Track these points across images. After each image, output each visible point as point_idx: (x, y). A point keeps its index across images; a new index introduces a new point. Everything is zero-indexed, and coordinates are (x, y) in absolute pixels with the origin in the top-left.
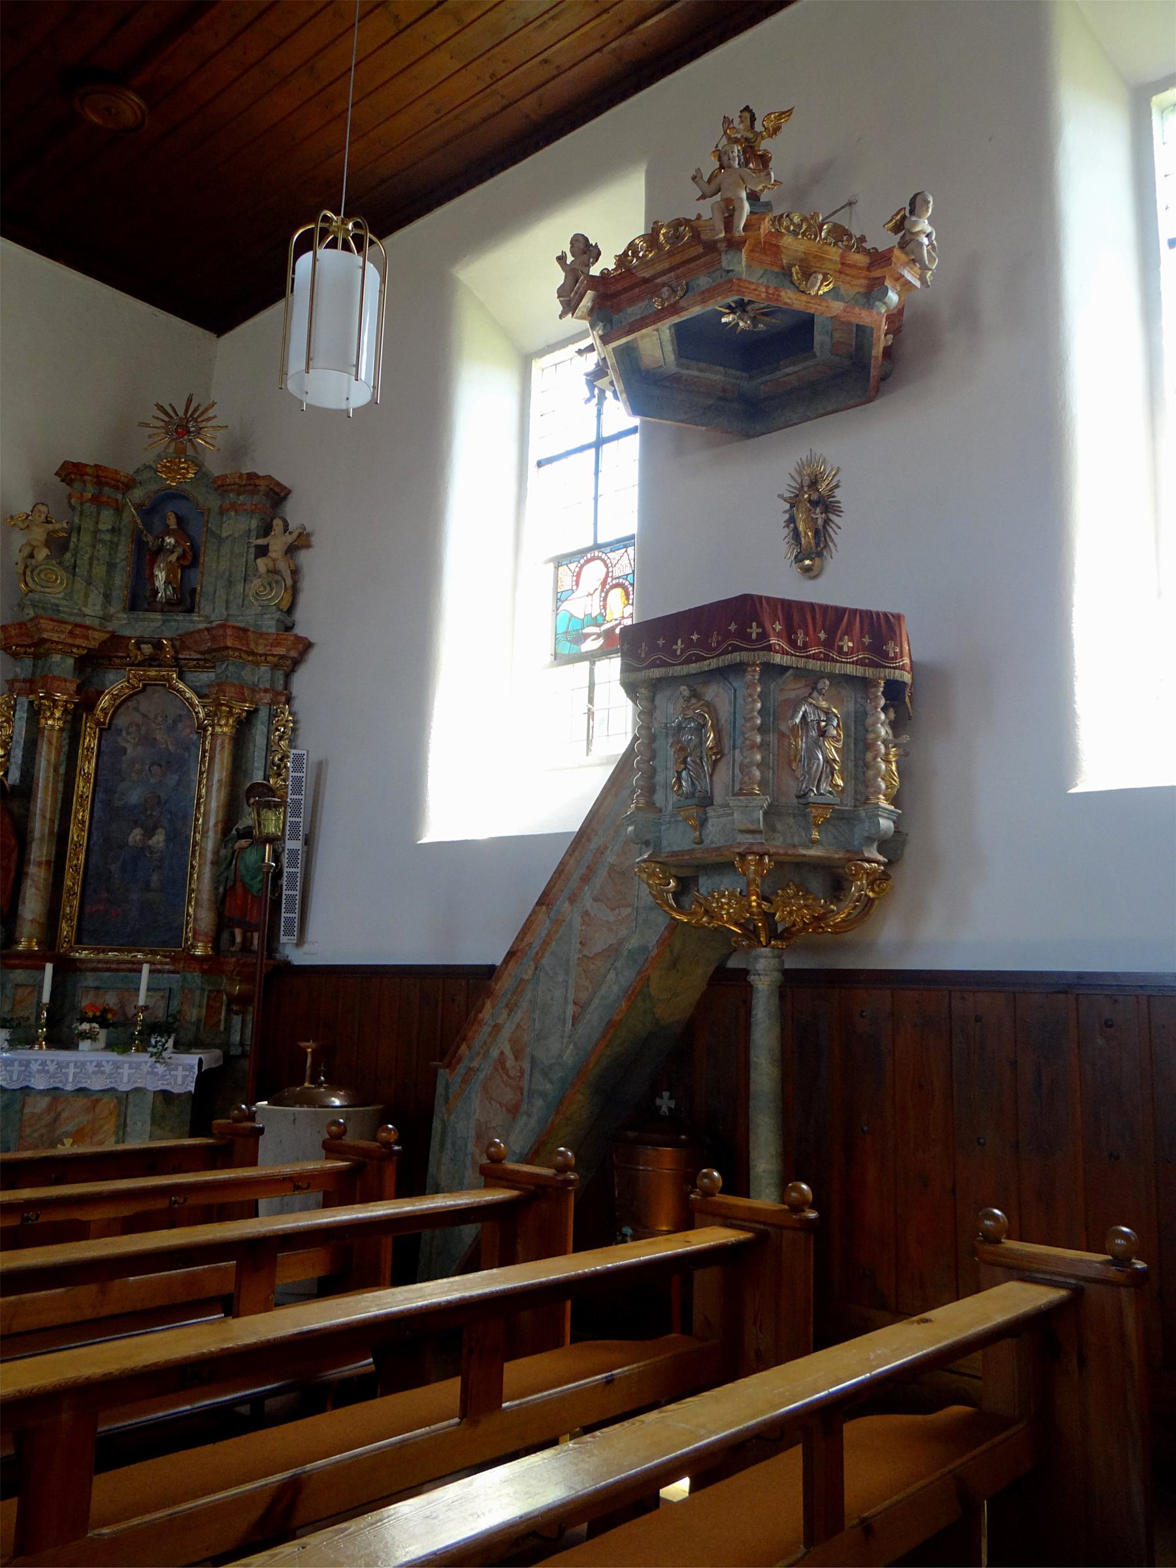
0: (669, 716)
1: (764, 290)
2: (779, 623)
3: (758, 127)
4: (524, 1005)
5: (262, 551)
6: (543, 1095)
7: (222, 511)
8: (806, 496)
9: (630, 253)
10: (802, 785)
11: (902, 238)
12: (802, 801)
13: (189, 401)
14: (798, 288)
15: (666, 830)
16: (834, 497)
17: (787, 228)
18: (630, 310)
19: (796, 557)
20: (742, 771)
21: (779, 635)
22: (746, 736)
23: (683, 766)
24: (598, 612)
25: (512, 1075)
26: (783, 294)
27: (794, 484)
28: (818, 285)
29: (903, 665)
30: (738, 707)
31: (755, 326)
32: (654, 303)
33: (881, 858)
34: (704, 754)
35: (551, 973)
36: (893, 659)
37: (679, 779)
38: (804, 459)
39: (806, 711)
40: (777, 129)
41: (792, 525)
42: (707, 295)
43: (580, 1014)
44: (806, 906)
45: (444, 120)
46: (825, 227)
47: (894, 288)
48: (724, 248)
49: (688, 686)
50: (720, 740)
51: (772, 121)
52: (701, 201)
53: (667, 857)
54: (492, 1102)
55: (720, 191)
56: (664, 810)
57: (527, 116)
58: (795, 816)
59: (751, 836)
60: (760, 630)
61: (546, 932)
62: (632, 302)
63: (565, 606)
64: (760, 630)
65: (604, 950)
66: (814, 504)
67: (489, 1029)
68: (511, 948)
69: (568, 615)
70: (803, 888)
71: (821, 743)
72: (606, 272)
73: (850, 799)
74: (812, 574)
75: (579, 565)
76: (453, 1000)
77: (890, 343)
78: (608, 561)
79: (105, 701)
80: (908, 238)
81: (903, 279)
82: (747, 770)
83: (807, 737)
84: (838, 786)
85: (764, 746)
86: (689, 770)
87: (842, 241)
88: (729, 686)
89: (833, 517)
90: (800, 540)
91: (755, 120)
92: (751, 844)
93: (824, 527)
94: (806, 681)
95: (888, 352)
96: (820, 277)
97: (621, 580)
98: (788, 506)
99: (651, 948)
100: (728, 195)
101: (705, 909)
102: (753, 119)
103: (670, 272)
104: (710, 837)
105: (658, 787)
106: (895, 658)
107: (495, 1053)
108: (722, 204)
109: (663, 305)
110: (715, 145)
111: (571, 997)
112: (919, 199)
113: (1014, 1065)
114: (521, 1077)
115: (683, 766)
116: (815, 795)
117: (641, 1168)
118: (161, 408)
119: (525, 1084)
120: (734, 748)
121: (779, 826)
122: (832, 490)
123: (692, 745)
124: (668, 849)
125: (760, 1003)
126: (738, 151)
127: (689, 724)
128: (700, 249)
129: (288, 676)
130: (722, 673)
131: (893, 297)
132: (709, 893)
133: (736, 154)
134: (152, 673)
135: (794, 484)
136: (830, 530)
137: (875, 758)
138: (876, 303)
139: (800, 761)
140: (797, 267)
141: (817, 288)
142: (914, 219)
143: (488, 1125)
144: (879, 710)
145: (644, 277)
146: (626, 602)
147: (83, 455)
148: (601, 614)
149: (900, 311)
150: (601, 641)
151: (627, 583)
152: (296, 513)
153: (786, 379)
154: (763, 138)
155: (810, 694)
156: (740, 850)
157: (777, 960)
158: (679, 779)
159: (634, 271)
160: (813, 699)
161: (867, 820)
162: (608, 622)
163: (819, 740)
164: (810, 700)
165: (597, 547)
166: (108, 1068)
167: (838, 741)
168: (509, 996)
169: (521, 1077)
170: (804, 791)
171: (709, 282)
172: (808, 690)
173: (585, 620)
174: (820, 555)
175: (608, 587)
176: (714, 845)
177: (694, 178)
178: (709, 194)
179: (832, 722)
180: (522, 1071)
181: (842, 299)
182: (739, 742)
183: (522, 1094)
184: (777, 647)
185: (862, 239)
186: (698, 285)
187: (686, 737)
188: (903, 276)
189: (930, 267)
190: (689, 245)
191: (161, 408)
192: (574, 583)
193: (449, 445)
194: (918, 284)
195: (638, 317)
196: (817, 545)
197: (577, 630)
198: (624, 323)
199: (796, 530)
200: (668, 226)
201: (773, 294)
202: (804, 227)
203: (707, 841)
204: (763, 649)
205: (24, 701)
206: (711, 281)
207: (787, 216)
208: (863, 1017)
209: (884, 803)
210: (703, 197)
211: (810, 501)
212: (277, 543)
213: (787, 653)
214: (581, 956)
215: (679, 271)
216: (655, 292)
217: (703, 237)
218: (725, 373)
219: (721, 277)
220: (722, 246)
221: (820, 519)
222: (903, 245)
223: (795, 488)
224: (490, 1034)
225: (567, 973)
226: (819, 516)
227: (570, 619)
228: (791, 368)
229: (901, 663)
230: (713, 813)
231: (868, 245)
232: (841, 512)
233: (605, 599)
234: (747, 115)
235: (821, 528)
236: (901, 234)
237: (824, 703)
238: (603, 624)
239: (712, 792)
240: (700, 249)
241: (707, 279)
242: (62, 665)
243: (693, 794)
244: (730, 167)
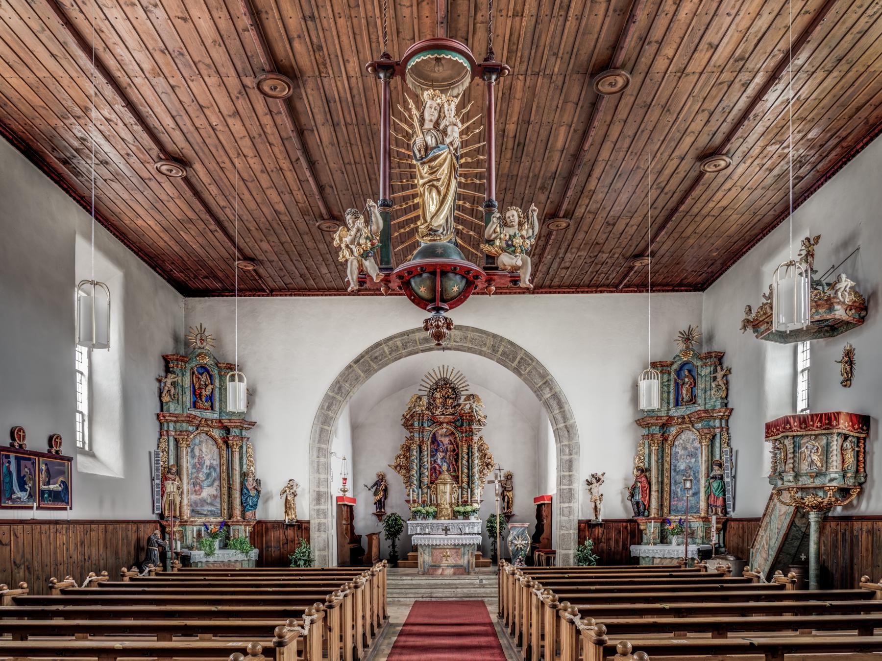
4: (768, 530)
5: (715, 379)
7: (702, 367)
13: (690, 327)
40: (818, 242)
62: (761, 325)
79: (671, 438)
118: (680, 333)
121: (800, 479)
129: (727, 421)
134: (684, 426)
147: (657, 359)
152: (726, 363)
166: (221, 555)
191: (680, 333)
205: (646, 442)
212: (720, 374)
242: (656, 430)
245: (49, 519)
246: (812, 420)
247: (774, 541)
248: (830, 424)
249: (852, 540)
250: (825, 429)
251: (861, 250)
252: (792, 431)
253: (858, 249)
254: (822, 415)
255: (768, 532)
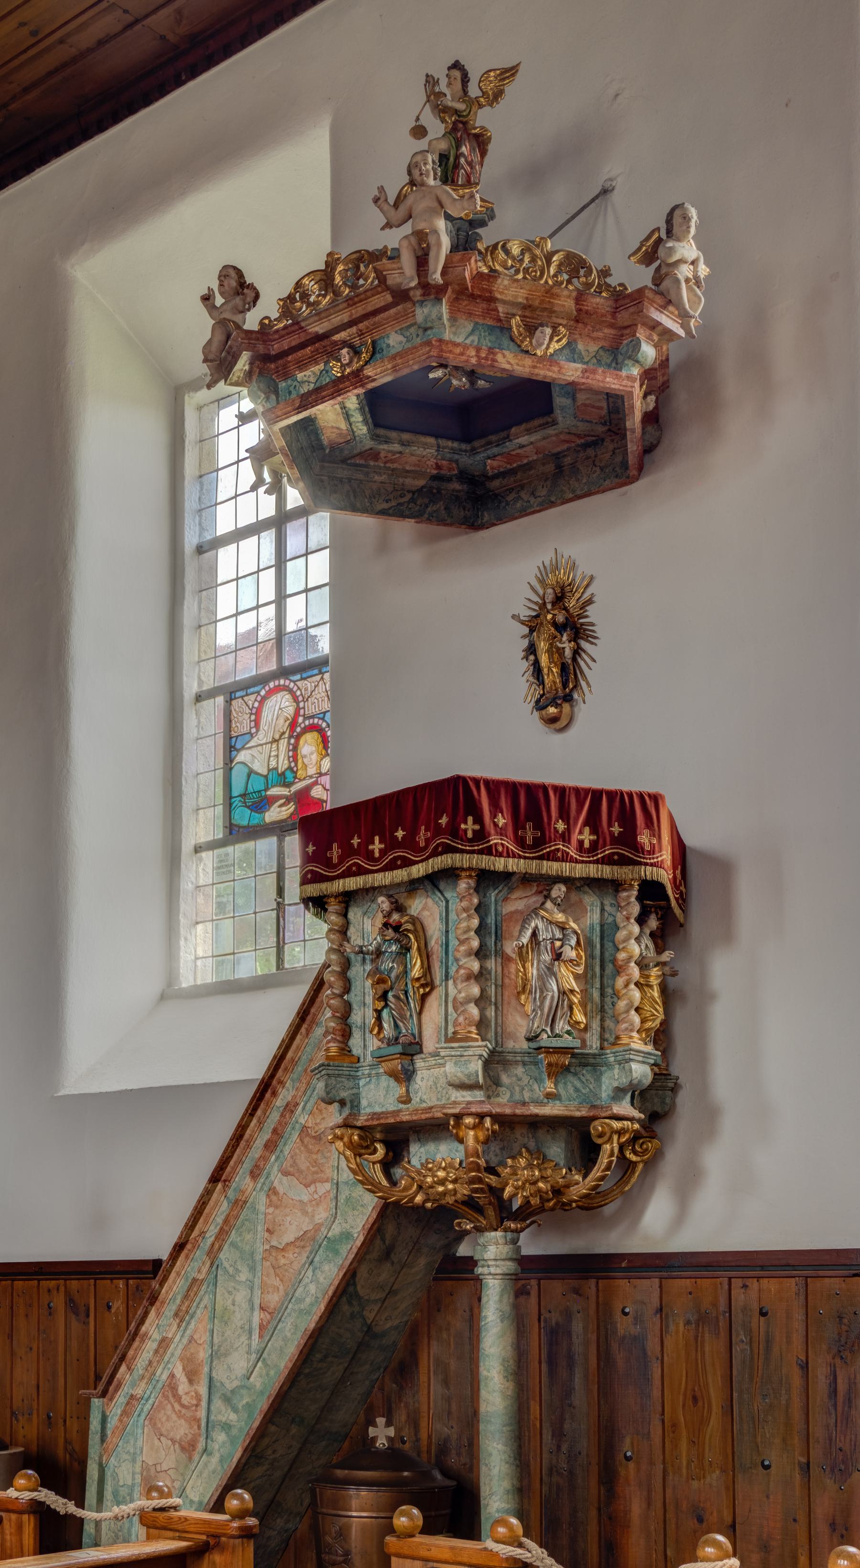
0: (365, 936)
1: (473, 353)
2: (503, 815)
3: (474, 91)
6: (226, 1427)
8: (549, 617)
9: (297, 296)
10: (533, 1024)
11: (658, 269)
12: (534, 1045)
14: (519, 346)
15: (364, 1085)
16: (587, 617)
17: (504, 265)
18: (300, 376)
19: (538, 702)
20: (455, 1008)
21: (501, 832)
22: (461, 963)
23: (382, 1004)
24: (286, 766)
25: (186, 1403)
26: (499, 357)
27: (536, 599)
28: (546, 342)
29: (662, 861)
30: (450, 924)
31: (472, 383)
32: (332, 368)
33: (636, 1114)
34: (410, 986)
35: (231, 1270)
36: (649, 853)
37: (379, 1019)
38: (547, 563)
39: (536, 927)
40: (498, 95)
41: (532, 657)
42: (399, 361)
43: (269, 1322)
44: (543, 1178)
45: (42, 45)
46: (555, 258)
47: (649, 338)
48: (419, 298)
49: (389, 897)
50: (429, 967)
51: (491, 82)
52: (387, 230)
53: (367, 1120)
54: (162, 1438)
55: (410, 217)
56: (362, 1060)
57: (163, 38)
58: (524, 1064)
59: (469, 1093)
60: (477, 827)
61: (223, 1217)
62: (302, 365)
63: (243, 756)
64: (477, 827)
65: (297, 1239)
66: (560, 628)
67: (155, 1345)
68: (180, 1238)
69: (246, 770)
70: (540, 1157)
71: (556, 969)
72: (267, 322)
73: (595, 1039)
74: (558, 725)
75: (259, 698)
76: (109, 1307)
77: (652, 406)
78: (298, 693)
80: (664, 271)
81: (660, 328)
82: (462, 1009)
83: (539, 961)
84: (578, 1023)
85: (480, 976)
86: (391, 1008)
87: (578, 278)
88: (439, 895)
89: (584, 644)
90: (543, 677)
91: (468, 81)
92: (469, 1103)
93: (574, 659)
94: (537, 886)
95: (651, 418)
96: (548, 331)
97: (316, 721)
98: (526, 630)
99: (356, 1235)
100: (421, 226)
101: (418, 1185)
102: (465, 79)
103: (351, 326)
104: (420, 1094)
105: (354, 1029)
106: (652, 852)
107: (163, 1375)
108: (413, 240)
109: (343, 372)
110: (415, 118)
111: (257, 1302)
112: (677, 220)
113: (805, 1367)
114: (197, 1406)
115: (382, 1004)
116: (549, 1037)
117: (354, 1514)
119: (202, 1414)
120: (447, 978)
121: (505, 1079)
122: (583, 607)
123: (393, 975)
124: (368, 1110)
125: (491, 1302)
126: (434, 162)
127: (390, 947)
128: (389, 298)
130: (433, 881)
131: (648, 352)
132: (422, 1165)
133: (429, 167)
135: (536, 599)
136: (582, 663)
137: (627, 985)
138: (626, 362)
139: (530, 992)
140: (518, 318)
141: (544, 346)
142: (670, 244)
143: (159, 1470)
144: (632, 921)
145: (317, 332)
146: (324, 752)
148: (290, 768)
149: (664, 363)
150: (291, 808)
151: (324, 725)
153: (519, 451)
154: (481, 106)
155: (543, 904)
156: (456, 1111)
157: (511, 1246)
158: (379, 1019)
159: (303, 324)
160: (546, 910)
161: (617, 1066)
162: (300, 780)
163: (553, 965)
164: (542, 913)
165: (284, 672)
167: (578, 965)
168: (178, 1301)
169: (197, 1406)
170: (535, 1032)
171: (401, 343)
172: (540, 899)
173: (270, 777)
174: (568, 698)
175: (298, 730)
176: (424, 1105)
177: (376, 200)
178: (397, 223)
179: (569, 940)
180: (198, 1398)
181: (581, 359)
182: (453, 970)
183: (199, 1427)
184: (500, 849)
185: (605, 273)
186: (388, 346)
187: (387, 964)
188: (661, 324)
189: (692, 312)
190: (373, 291)
192: (253, 724)
193: (72, 528)
194: (681, 333)
195: (312, 386)
196: (565, 685)
197: (259, 792)
198: (294, 395)
199: (536, 665)
200: (346, 261)
201: (486, 359)
202: (527, 259)
203: (415, 1100)
204: (481, 852)
206: (404, 340)
207: (504, 246)
208: (626, 1314)
209: (637, 1044)
210: (388, 225)
211: (555, 624)
213: (514, 856)
214: (267, 1247)
215: (361, 325)
216: (332, 353)
217: (389, 282)
218: (439, 446)
219: (418, 335)
220: (417, 294)
221: (568, 648)
222: (658, 279)
223: (536, 603)
224: (156, 1352)
225: (252, 1269)
226: (566, 645)
227: (249, 776)
228: (526, 437)
229: (660, 859)
230: (423, 1064)
231: (612, 281)
232: (595, 638)
233: (295, 748)
234: (457, 74)
235: (570, 661)
236: (656, 264)
237: (560, 915)
238: (293, 783)
239: (420, 1033)
240: (389, 298)
241: (401, 338)
243: (397, 1039)
244: (423, 184)
245: (809, 1248)
246: (564, 814)
247: (239, 1363)
248: (628, 838)
249: (605, 1357)
250: (608, 861)
251: (616, 197)
252: (489, 851)
253: (605, 192)
254: (597, 795)
255: (198, 1325)
